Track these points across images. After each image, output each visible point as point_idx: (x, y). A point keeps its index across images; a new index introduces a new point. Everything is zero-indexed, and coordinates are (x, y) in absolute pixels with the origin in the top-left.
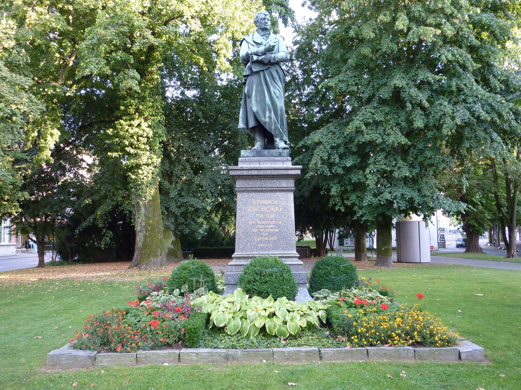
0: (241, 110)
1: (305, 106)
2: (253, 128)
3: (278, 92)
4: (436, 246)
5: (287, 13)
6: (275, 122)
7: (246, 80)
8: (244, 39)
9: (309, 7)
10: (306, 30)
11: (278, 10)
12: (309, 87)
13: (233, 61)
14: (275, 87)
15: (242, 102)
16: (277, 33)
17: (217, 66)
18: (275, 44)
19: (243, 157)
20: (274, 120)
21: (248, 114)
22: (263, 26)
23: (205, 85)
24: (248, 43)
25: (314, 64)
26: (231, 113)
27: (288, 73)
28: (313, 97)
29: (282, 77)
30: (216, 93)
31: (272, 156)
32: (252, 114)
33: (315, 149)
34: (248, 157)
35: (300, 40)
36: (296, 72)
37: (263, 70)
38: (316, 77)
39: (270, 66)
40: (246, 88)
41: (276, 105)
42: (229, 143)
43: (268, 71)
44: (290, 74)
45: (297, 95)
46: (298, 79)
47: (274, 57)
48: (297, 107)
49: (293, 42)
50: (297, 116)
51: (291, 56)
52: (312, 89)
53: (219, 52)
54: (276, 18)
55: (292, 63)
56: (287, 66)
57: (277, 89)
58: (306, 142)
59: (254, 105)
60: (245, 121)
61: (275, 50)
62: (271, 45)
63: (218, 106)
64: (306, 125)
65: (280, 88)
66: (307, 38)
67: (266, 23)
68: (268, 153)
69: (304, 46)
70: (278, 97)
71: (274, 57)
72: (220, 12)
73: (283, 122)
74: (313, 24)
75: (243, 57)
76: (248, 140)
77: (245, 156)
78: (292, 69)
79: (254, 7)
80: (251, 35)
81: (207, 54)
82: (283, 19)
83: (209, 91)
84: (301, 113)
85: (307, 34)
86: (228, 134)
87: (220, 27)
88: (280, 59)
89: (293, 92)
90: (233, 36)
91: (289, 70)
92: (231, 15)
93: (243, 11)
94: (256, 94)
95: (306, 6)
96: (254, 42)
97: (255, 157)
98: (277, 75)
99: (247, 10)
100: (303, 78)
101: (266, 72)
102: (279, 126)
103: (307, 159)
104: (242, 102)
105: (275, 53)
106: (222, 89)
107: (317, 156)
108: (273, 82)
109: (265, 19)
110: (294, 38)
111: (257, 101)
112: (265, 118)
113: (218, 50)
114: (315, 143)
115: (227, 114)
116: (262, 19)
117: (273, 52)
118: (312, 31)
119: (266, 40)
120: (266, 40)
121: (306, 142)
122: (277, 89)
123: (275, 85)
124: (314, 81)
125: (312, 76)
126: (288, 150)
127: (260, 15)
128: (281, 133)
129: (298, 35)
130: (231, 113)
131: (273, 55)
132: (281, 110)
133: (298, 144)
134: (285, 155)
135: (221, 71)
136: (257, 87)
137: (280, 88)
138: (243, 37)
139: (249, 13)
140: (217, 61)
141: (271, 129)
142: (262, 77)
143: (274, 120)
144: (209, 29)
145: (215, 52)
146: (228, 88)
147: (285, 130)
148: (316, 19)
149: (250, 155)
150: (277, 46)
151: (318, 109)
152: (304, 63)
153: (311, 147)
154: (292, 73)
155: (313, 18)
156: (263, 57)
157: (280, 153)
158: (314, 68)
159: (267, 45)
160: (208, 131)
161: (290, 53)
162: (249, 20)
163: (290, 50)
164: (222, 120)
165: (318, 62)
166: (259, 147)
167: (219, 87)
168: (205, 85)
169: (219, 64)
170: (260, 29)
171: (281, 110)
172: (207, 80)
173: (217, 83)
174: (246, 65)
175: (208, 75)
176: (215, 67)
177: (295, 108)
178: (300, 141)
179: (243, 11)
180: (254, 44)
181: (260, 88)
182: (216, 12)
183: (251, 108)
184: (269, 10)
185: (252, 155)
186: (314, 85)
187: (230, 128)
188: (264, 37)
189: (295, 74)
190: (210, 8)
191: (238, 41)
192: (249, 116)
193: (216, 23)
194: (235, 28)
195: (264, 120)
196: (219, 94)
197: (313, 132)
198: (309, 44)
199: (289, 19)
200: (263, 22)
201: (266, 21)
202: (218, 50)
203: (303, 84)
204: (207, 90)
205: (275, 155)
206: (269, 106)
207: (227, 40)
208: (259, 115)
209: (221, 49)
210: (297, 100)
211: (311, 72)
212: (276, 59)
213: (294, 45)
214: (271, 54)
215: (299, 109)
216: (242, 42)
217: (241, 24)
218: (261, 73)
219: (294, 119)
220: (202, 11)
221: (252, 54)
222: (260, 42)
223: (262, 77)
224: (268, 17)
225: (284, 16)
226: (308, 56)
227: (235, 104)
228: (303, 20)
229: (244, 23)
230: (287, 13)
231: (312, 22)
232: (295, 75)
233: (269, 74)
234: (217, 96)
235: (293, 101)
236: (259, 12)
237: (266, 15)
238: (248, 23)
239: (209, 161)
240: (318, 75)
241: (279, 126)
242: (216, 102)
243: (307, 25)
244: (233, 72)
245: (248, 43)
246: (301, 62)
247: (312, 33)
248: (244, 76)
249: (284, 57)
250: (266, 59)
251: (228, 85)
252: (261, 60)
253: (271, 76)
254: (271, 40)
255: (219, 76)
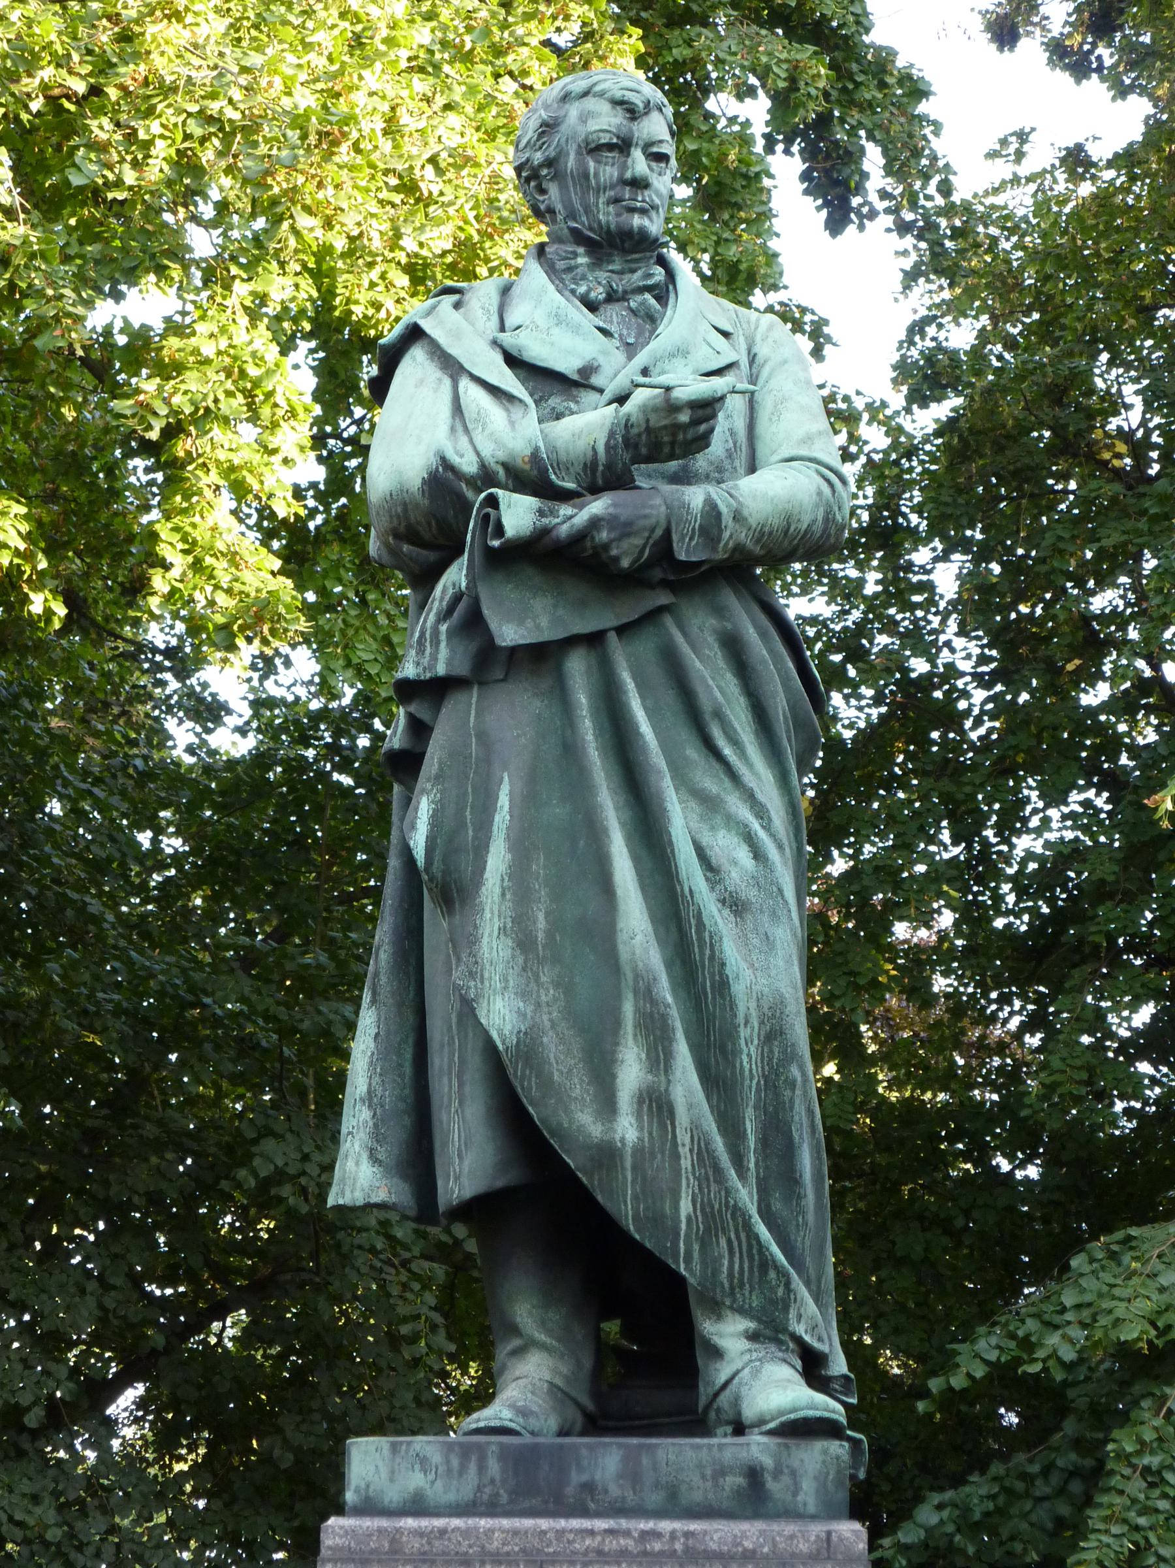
0: (368, 1021)
1: (1024, 982)
2: (468, 1210)
3: (743, 855)
4: (951, 177)
5: (848, 99)
6: (704, 1153)
7: (419, 730)
8: (415, 334)
9: (1059, 52)
10: (1033, 255)
11: (764, 74)
12: (1054, 795)
13: (320, 537)
14: (710, 804)
15: (384, 935)
16: (752, 280)
17: (160, 582)
18: (718, 384)
19: (369, 1508)
20: (695, 1128)
21: (438, 1061)
22: (607, 215)
23: (42, 755)
24: (452, 367)
25: (1105, 581)
26: (286, 1032)
27: (856, 655)
28: (1100, 892)
29: (780, 706)
30: (144, 838)
31: (674, 1507)
32: (476, 1061)
33: (1124, 1419)
34: (417, 1506)
35: (977, 353)
36: (929, 651)
37: (594, 640)
38: (1124, 705)
39: (664, 598)
40: (424, 809)
41: (723, 986)
42: (247, 1338)
43: (646, 646)
44: (869, 674)
45: (942, 873)
46: (950, 718)
47: (712, 509)
48: (941, 983)
49: (903, 369)
50: (946, 1079)
51: (887, 502)
52: (1088, 818)
53: (181, 448)
54: (745, 140)
55: (895, 568)
56: (846, 592)
57: (731, 822)
58: (1027, 1345)
59: (493, 976)
60: (399, 1131)
61: (718, 446)
62: (682, 394)
63: (157, 961)
64: (1033, 1172)
65: (760, 811)
66: (1044, 332)
67: (639, 184)
68: (631, 1474)
69: (1010, 409)
70: (736, 906)
71: (712, 509)
72: (203, 76)
73: (789, 1153)
74: (1103, 199)
75: (399, 504)
76: (446, 1306)
77: (393, 1495)
78: (890, 626)
79: (536, 33)
80: (484, 292)
81: (75, 466)
82: (809, 154)
83: (76, 814)
84: (983, 1048)
85: (1042, 301)
86: (249, 1247)
87: (207, 211)
88: (762, 535)
89: (904, 846)
90: (327, 294)
91: (861, 629)
92: (305, 100)
93: (425, 66)
94: (518, 876)
95: (1031, 48)
96: (513, 361)
97: (492, 1509)
98: (731, 683)
99: (467, 58)
100: (1001, 708)
101: (620, 655)
102: (746, 1196)
103: (1042, 1514)
104: (384, 935)
105: (718, 475)
106: (202, 796)
107: (1136, 1487)
108: (693, 752)
109: (623, 146)
110: (917, 328)
111: (524, 943)
112: (608, 1106)
113: (173, 431)
114: (1124, 1351)
115: (247, 1047)
116: (595, 149)
117: (701, 462)
118: (1086, 269)
119: (631, 350)
120: (631, 350)
121: (1027, 1345)
122: (731, 822)
123: (711, 782)
124: (1112, 745)
125: (1096, 695)
126: (838, 1449)
127: (573, 111)
128: (765, 1263)
129: (957, 309)
130: (286, 1032)
131: (695, 496)
132: (774, 1034)
133: (947, 1364)
134: (808, 1497)
135: (195, 627)
136: (527, 803)
137: (760, 811)
138: (414, 309)
139: (487, 84)
140: (164, 530)
141: (663, 1223)
142: (582, 699)
143: (695, 1128)
144: (88, 232)
145: (148, 448)
146: (262, 789)
147: (804, 1241)
148: (1127, 159)
149: (439, 1491)
150: (735, 406)
151: (1144, 1015)
152: (1012, 568)
153: (1078, 1397)
154: (894, 662)
155: (1100, 152)
156: (598, 506)
157: (754, 1474)
158: (1114, 617)
159: (640, 396)
160: (51, 1208)
161: (873, 471)
162: (481, 152)
163: (876, 438)
164: (192, 1101)
165: (1150, 564)
166: (538, 1403)
167: (174, 775)
168: (42, 755)
169: (179, 562)
170: (578, 237)
171: (774, 1034)
172: (65, 711)
173: (159, 737)
174: (425, 579)
175: (68, 663)
176: (138, 587)
177: (919, 993)
178: (968, 1336)
179: (425, 66)
180: (508, 381)
181: (557, 811)
182: (164, 66)
183: (468, 1010)
184: (680, 67)
185: (465, 1489)
186: (1113, 782)
187: (265, 1184)
188: (614, 315)
189: (919, 666)
190: (105, 37)
191: (368, 345)
192: (443, 1086)
193: (157, 169)
194: (350, 221)
195: (596, 1130)
196: (172, 844)
197: (1097, 1247)
198: (1056, 394)
199: (873, 158)
200: (609, 172)
201: (639, 164)
202: (173, 431)
203: (1005, 769)
204: (55, 807)
205: (698, 1491)
206: (646, 993)
207: (262, 341)
208: (546, 1083)
209: (205, 416)
210: (946, 919)
211: (1074, 651)
212: (731, 534)
213: (919, 398)
214: (684, 478)
215: (957, 1006)
216: (391, 359)
217: (409, 187)
218: (577, 666)
219: (911, 1107)
220: (31, 64)
221: (486, 477)
222: (567, 365)
223: (582, 699)
224: (657, 127)
225: (824, 121)
226: (1047, 500)
227: (330, 945)
228: (1003, 170)
229: (428, 182)
230: (848, 99)
231: (1086, 189)
232: (926, 683)
233: (656, 673)
234: (155, 859)
235: (901, 930)
236: (577, 82)
237: (633, 113)
238: (473, 183)
239: (47, 1512)
240: (1143, 686)
241: (746, 1196)
242: (138, 925)
243: (1042, 207)
244: (319, 641)
245: (452, 367)
246: (983, 554)
247: (1089, 283)
248: (407, 690)
249: (809, 516)
250: (624, 528)
251: (260, 760)
252: (581, 536)
253: (669, 698)
254: (680, 352)
255: (182, 674)
